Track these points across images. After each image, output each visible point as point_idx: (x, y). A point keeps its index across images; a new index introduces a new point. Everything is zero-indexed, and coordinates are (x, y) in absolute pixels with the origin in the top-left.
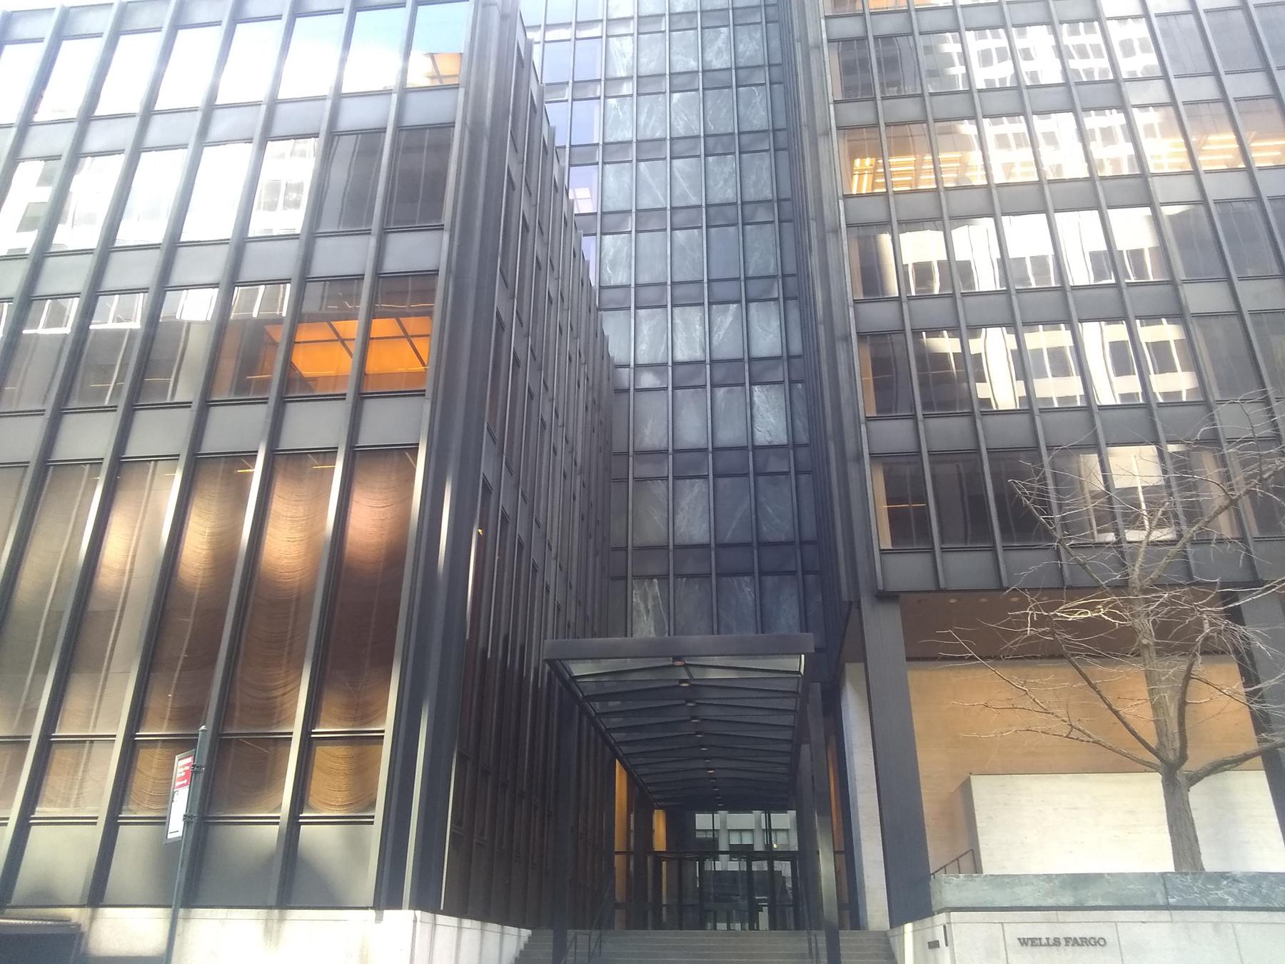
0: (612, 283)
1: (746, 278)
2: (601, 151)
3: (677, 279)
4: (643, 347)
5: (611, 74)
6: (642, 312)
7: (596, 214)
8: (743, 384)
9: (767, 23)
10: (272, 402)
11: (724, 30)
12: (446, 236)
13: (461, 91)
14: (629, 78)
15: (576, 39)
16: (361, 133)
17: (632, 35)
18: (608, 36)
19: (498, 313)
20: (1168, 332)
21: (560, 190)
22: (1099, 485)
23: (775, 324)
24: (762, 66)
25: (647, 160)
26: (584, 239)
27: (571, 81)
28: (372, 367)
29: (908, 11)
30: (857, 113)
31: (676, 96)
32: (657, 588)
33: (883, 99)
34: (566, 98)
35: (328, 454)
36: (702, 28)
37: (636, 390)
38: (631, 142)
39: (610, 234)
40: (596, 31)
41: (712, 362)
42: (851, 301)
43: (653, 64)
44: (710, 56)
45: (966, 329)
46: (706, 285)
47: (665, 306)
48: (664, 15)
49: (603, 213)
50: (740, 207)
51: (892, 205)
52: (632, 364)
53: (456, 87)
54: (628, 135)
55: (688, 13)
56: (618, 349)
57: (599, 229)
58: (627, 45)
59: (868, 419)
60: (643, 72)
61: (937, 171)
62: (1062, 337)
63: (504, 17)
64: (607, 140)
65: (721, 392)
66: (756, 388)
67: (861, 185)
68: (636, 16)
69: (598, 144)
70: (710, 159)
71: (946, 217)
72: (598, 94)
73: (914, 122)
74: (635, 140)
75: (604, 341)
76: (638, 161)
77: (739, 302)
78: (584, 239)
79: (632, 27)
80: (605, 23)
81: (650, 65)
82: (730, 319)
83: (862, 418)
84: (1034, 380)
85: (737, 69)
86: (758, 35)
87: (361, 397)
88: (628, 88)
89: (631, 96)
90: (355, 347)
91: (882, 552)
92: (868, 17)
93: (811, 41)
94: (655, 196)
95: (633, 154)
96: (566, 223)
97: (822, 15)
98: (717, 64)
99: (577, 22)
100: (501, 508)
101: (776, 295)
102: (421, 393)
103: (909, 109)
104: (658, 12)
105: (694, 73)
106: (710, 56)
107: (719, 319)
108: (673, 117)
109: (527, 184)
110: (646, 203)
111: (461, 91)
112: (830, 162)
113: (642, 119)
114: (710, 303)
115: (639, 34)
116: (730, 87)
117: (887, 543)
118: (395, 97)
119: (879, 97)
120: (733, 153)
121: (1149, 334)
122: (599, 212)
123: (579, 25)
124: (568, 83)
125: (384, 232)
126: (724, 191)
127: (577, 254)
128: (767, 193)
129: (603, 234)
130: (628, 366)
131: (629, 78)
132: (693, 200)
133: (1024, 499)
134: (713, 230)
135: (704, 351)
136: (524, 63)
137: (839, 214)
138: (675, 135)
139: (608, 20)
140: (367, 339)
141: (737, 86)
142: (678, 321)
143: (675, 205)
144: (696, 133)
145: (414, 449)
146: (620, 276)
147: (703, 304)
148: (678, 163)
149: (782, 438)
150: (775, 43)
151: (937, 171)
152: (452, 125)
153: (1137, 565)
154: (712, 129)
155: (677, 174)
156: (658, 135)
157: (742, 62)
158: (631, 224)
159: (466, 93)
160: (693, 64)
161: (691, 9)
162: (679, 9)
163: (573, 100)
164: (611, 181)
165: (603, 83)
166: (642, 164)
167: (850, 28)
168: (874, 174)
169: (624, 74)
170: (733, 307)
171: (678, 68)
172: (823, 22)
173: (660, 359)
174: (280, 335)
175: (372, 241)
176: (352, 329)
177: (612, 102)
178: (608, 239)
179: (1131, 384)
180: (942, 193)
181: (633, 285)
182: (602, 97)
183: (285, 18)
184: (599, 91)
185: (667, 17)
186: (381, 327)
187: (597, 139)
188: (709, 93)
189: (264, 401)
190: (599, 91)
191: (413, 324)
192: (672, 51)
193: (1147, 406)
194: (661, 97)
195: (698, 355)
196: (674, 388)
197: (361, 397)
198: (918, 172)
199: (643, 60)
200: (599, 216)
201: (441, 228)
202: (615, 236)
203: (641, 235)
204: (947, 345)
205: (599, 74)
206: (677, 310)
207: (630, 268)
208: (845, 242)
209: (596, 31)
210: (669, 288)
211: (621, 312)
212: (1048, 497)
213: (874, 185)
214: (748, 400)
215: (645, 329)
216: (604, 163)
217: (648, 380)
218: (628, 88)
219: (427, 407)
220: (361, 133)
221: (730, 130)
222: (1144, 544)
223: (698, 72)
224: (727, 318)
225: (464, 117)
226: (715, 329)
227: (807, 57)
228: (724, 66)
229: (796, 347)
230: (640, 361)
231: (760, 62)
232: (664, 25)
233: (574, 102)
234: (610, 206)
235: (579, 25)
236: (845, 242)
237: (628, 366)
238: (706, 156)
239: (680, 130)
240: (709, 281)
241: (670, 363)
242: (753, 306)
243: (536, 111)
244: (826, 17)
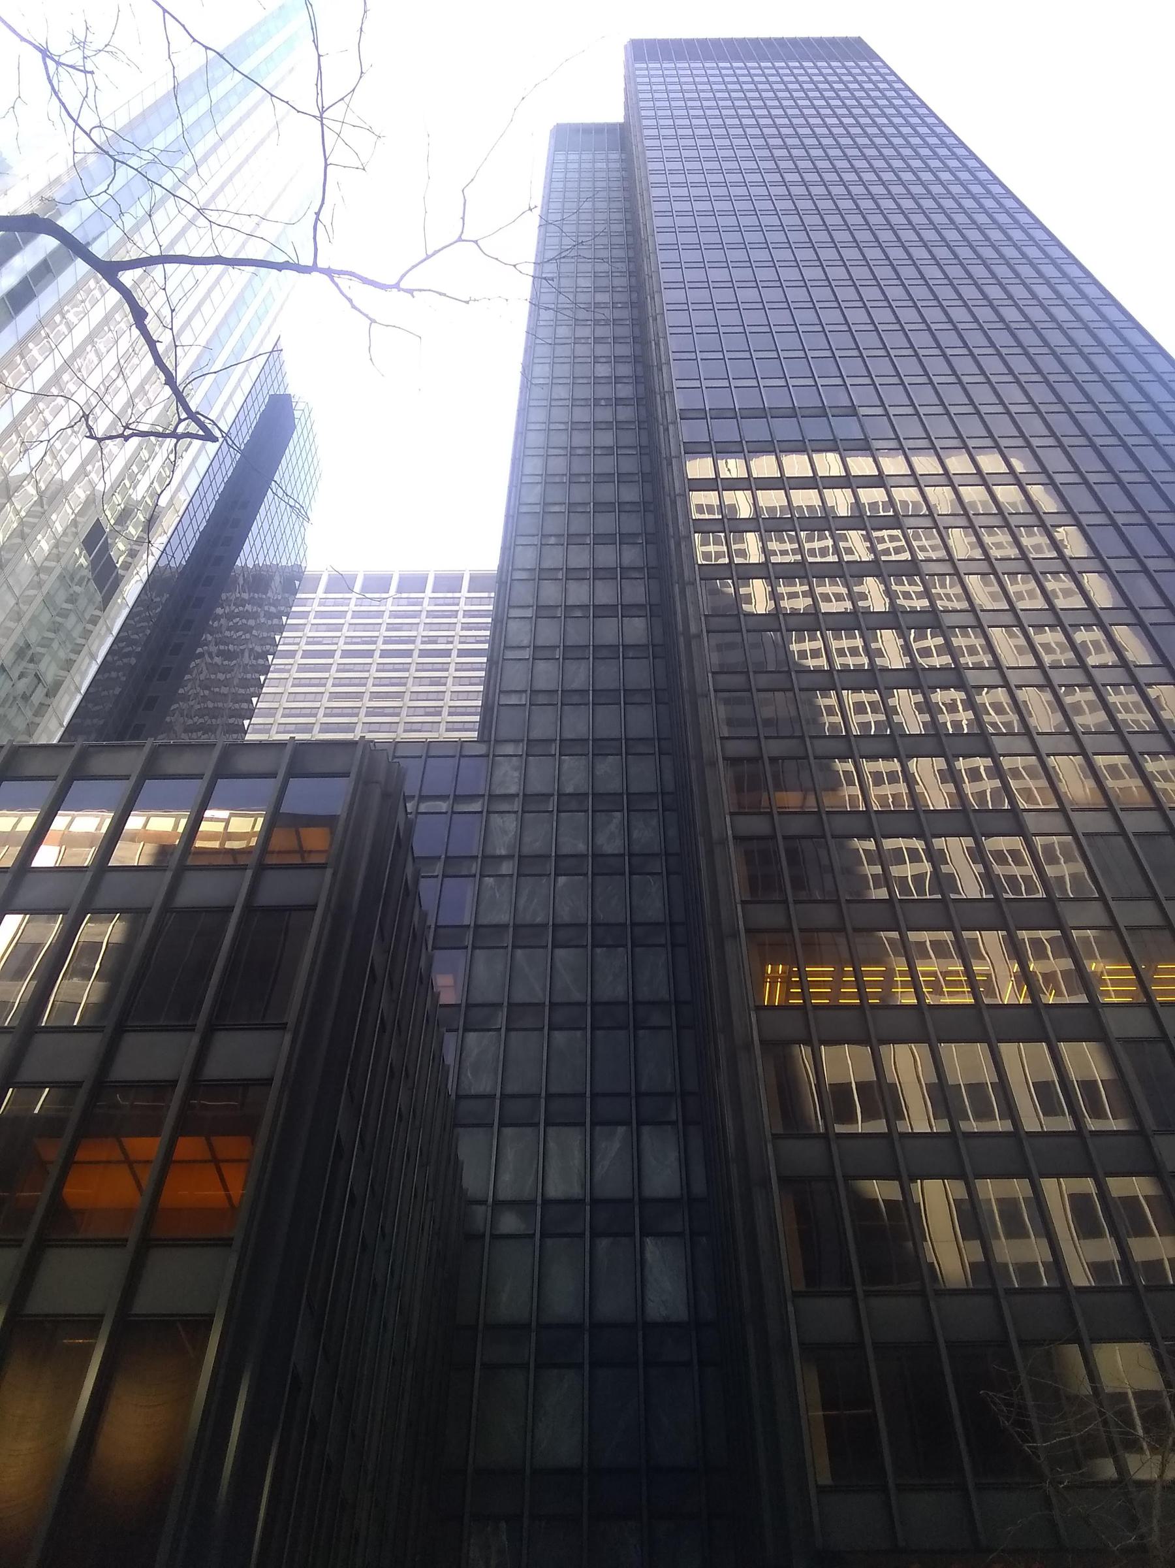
0: (473, 1092)
1: (639, 1094)
2: (472, 933)
3: (553, 1090)
4: (506, 1177)
5: (489, 851)
6: (508, 1131)
7: (459, 1005)
8: (631, 1235)
9: (663, 811)
10: (27, 1246)
11: (618, 814)
12: (288, 1038)
13: (329, 872)
14: (509, 857)
15: (453, 813)
16: (206, 911)
17: (516, 812)
18: (488, 812)
19: (338, 1136)
20: (1139, 1187)
21: (425, 982)
22: (1086, 1389)
23: (673, 1156)
24: (657, 855)
25: (525, 947)
26: (447, 1035)
27: (443, 856)
28: (168, 1198)
29: (818, 813)
30: (767, 916)
31: (562, 880)
32: (504, 1538)
33: (796, 902)
34: (436, 874)
35: (91, 1324)
36: (593, 811)
37: (495, 1237)
38: (507, 926)
39: (475, 1030)
40: (476, 806)
41: (595, 1202)
42: (769, 1137)
43: (538, 844)
44: (601, 839)
45: (906, 1176)
46: (588, 1100)
47: (537, 1125)
48: (553, 795)
49: (468, 1006)
50: (631, 1007)
51: (812, 1023)
52: (490, 1200)
53: (322, 867)
54: (504, 917)
55: (579, 794)
56: (473, 1181)
57: (461, 1023)
58: (510, 824)
59: (796, 1294)
60: (526, 851)
61: (860, 984)
62: (1019, 1188)
63: (386, 795)
64: (480, 922)
65: (603, 1243)
66: (648, 1240)
67: (772, 995)
68: (521, 794)
69: (468, 926)
70: (598, 950)
71: (744, 630)
72: (473, 872)
73: (827, 930)
74: (511, 924)
75: (455, 1167)
76: (514, 947)
77: (629, 1124)
78: (447, 1035)
79: (516, 805)
80: (486, 798)
81: (535, 842)
82: (617, 1145)
83: (788, 1292)
84: (993, 1242)
85: (630, 855)
86: (654, 822)
87: (147, 1243)
88: (507, 868)
89: (511, 876)
90: (147, 1177)
91: (821, 1490)
92: (776, 816)
93: (715, 835)
94: (531, 988)
95: (508, 940)
96: (427, 1020)
97: (727, 811)
98: (609, 849)
99: (455, 795)
100: (310, 1415)
101: (674, 1118)
102: (227, 1243)
103: (825, 915)
104: (545, 791)
105: (581, 857)
106: (601, 839)
107: (603, 1145)
108: (557, 901)
109: (390, 979)
110: (520, 996)
111: (329, 872)
112: (739, 967)
113: (522, 901)
114: (593, 1124)
115: (523, 812)
116: (623, 874)
117: (825, 1479)
118: (249, 873)
119: (790, 899)
120: (625, 946)
121: (1118, 1186)
122: (464, 1005)
123: (458, 798)
124: (440, 857)
125: (212, 1029)
126: (613, 987)
127: (439, 1057)
128: (664, 994)
129: (466, 1030)
130: (483, 1202)
131: (509, 857)
132: (577, 996)
133: (1001, 1419)
134: (599, 1033)
135: (584, 1186)
136: (403, 842)
137: (752, 1029)
138: (558, 921)
139: (490, 795)
140: (168, 1160)
141: (630, 874)
142: (552, 1145)
143: (556, 999)
144: (583, 921)
145: (206, 1322)
146: (483, 1084)
147: (584, 1124)
148: (560, 953)
149: (681, 1313)
150: (673, 832)
151: (860, 984)
152: (313, 908)
153: (1155, 1521)
154: (601, 917)
155: (558, 965)
156: (539, 920)
157: (636, 849)
158: (501, 1019)
159: (334, 874)
160: (581, 847)
161: (582, 791)
162: (569, 789)
163: (444, 876)
164: (480, 969)
165: (479, 860)
166: (519, 952)
167: (756, 825)
168: (788, 984)
169: (503, 852)
170: (621, 1130)
171: (565, 850)
172: (728, 818)
173: (526, 1194)
174: (53, 1152)
175: (195, 1039)
176: (148, 1147)
177: (489, 881)
178: (472, 1037)
179: (1106, 1249)
180: (867, 1012)
181: (498, 1095)
182: (478, 876)
183: (133, 779)
184: (475, 868)
185: (556, 797)
186: (188, 1147)
187: (467, 920)
188: (598, 878)
189: (18, 1244)
190: (475, 868)
191: (228, 1146)
192: (559, 832)
193: (1132, 1287)
194: (544, 880)
195: (576, 1191)
196: (542, 1236)
197: (147, 1243)
198: (837, 984)
199: (527, 839)
200: (463, 1009)
201: (283, 1027)
202: (482, 1033)
203: (513, 1034)
204: (880, 1190)
205: (475, 851)
206: (552, 1131)
207: (496, 1074)
208: (759, 1062)
209: (476, 806)
210: (543, 1101)
211: (481, 1129)
212: (1028, 1416)
213: (788, 995)
214: (638, 1257)
215: (510, 1155)
216: (474, 948)
217: (510, 1223)
218: (507, 868)
219: (233, 1261)
220: (206, 911)
221: (622, 920)
222: (1158, 1486)
223: (587, 856)
224: (613, 1144)
225: (329, 901)
226: (598, 1158)
227: (710, 853)
228: (616, 852)
229: (699, 1187)
230: (502, 1196)
231: (656, 849)
232: (552, 805)
233: (445, 879)
234: (477, 998)
235: (458, 798)
236: (759, 1062)
237: (483, 1202)
238: (593, 946)
239: (565, 916)
240: (593, 1095)
241: (539, 1201)
242: (646, 1130)
243: (411, 893)
244: (731, 814)
